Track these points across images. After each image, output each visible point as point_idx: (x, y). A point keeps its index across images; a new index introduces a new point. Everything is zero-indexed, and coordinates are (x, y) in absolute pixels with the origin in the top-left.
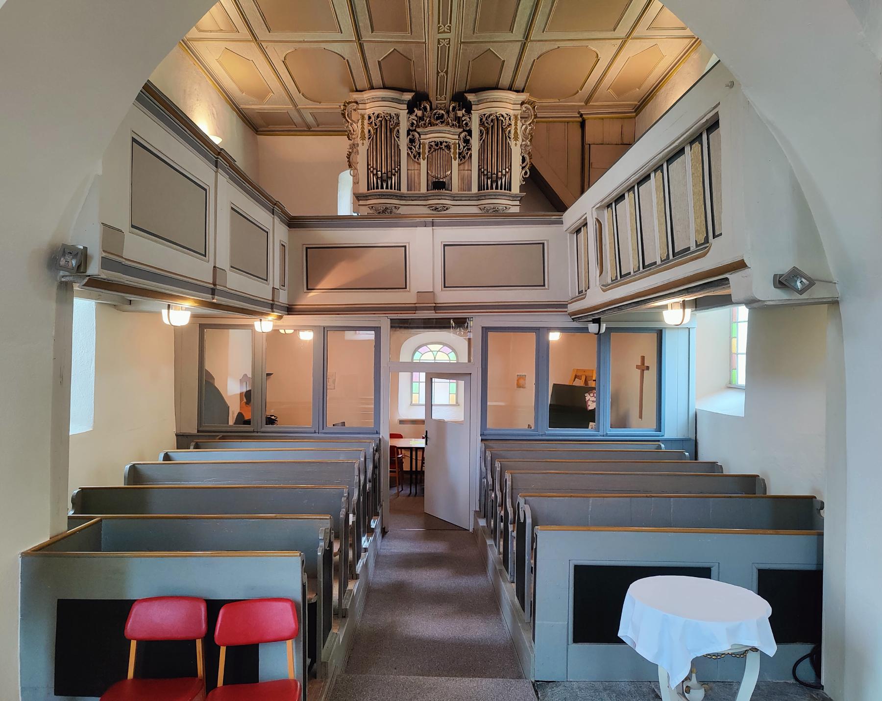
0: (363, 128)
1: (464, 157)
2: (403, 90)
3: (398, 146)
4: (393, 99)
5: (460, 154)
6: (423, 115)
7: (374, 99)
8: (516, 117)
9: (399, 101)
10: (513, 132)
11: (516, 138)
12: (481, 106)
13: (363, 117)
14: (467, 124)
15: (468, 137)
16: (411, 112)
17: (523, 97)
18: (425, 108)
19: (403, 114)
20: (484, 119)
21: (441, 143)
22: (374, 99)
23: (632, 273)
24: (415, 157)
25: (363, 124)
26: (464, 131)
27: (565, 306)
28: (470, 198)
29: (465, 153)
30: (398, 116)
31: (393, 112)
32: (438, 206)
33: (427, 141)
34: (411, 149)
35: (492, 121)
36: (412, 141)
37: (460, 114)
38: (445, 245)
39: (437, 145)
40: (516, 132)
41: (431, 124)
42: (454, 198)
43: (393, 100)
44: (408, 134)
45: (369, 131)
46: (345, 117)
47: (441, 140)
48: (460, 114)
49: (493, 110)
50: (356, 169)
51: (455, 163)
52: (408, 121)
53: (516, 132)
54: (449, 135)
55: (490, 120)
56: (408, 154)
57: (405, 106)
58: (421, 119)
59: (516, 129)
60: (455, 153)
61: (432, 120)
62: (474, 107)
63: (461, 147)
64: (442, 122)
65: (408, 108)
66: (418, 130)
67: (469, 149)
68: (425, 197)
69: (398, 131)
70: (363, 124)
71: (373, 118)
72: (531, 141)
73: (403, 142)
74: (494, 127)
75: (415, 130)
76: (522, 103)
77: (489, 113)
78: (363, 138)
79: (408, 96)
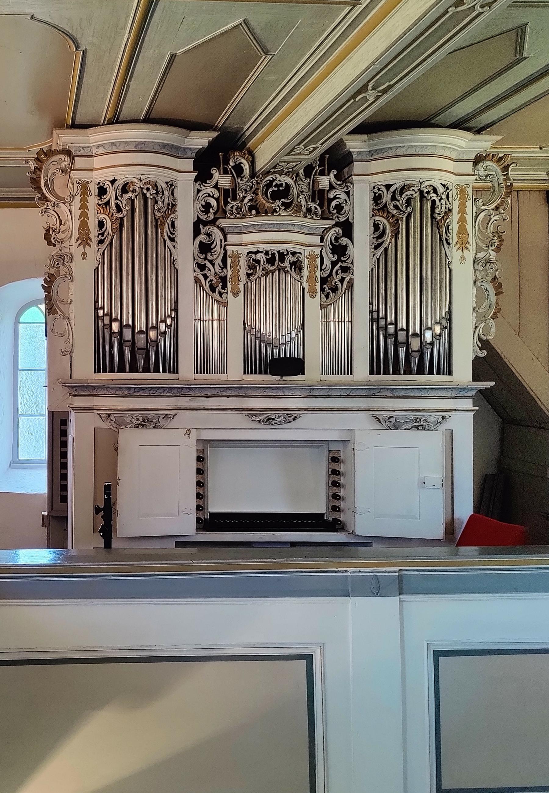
0: (84, 216)
3: (173, 262)
4: (164, 146)
5: (324, 281)
7: (116, 149)
8: (462, 191)
9: (175, 151)
10: (454, 227)
11: (463, 244)
12: (375, 166)
13: (84, 188)
14: (339, 208)
15: (344, 241)
16: (203, 176)
17: (484, 143)
18: (239, 169)
19: (186, 182)
20: (387, 197)
21: (282, 257)
22: (116, 149)
23: (313, 373)
24: (213, 289)
25: (84, 206)
28: (350, 392)
30: (171, 185)
31: (161, 178)
32: (273, 414)
34: (202, 267)
35: (408, 202)
36: (205, 248)
37: (323, 182)
38: (438, 654)
39: (271, 261)
40: (462, 230)
41: (256, 208)
42: (312, 392)
44: (197, 232)
45: (101, 224)
46: (38, 188)
47: (282, 248)
48: (323, 182)
49: (412, 177)
50: (66, 317)
52: (197, 197)
53: (462, 230)
54: (299, 234)
55: (403, 200)
57: (189, 164)
58: (228, 194)
59: (462, 220)
60: (311, 279)
61: (261, 198)
62: (358, 167)
64: (287, 206)
65: (195, 168)
66: (223, 223)
67: (345, 270)
68: (239, 391)
69: (173, 225)
70: (84, 206)
71: (111, 194)
72: (498, 250)
73: (186, 249)
74: (408, 213)
75: (213, 222)
76: (478, 160)
78: (84, 240)
79: (200, 140)
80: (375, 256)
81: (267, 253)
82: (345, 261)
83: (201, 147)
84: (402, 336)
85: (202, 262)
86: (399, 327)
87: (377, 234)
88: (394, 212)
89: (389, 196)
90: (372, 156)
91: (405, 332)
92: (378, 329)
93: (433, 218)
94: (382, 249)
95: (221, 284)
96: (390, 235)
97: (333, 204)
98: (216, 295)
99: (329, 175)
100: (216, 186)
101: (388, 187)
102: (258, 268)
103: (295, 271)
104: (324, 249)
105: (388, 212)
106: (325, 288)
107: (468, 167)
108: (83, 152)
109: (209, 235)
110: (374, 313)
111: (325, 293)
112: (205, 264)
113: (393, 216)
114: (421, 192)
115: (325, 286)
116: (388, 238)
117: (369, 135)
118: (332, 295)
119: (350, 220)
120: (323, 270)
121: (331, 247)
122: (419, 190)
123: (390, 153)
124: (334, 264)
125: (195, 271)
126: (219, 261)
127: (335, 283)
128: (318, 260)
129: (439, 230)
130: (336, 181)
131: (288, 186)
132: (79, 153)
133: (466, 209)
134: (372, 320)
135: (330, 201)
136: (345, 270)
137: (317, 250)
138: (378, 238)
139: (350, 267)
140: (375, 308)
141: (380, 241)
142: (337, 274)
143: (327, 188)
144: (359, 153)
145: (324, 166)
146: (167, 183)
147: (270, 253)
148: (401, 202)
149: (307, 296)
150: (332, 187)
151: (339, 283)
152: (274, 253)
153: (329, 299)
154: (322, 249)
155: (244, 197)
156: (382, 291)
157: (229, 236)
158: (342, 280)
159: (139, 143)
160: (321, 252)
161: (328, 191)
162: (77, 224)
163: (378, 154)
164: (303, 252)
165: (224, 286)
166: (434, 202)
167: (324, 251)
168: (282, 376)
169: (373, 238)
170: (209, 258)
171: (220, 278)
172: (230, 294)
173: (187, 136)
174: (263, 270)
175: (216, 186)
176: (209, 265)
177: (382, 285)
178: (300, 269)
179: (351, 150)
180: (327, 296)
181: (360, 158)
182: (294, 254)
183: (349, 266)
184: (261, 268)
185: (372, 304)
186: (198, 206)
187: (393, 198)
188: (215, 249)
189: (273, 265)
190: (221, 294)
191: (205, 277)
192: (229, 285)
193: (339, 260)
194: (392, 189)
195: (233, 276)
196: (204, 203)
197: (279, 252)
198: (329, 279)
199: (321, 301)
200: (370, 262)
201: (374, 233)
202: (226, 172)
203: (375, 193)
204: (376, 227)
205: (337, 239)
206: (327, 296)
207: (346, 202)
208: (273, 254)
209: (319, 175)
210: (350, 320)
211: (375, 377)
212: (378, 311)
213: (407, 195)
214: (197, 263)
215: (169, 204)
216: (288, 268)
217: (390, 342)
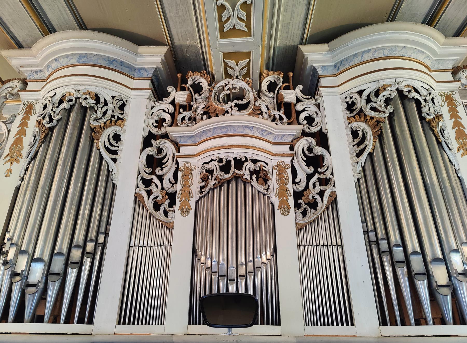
1: (311, 202)
2: (139, 40)
4: (112, 61)
5: (298, 195)
6: (191, 98)
14: (310, 120)
15: (319, 150)
16: (159, 93)
20: (361, 103)
21: (239, 163)
24: (157, 206)
26: (304, 134)
27: (213, 131)
29: (313, 192)
33: (197, 163)
34: (147, 183)
35: (388, 101)
36: (154, 163)
37: (289, 96)
39: (226, 168)
43: (112, 64)
44: (147, 142)
47: (240, 154)
48: (289, 96)
49: (385, 78)
51: (286, 224)
56: (137, 197)
57: (147, 84)
60: (282, 193)
61: (215, 104)
62: (324, 82)
63: (301, 175)
64: (241, 108)
67: (325, 182)
69: (117, 137)
73: (128, 167)
75: (165, 136)
77: (374, 87)
80: (359, 164)
81: (220, 161)
82: (323, 173)
83: (155, 66)
84: (417, 263)
85: (148, 177)
86: (410, 249)
87: (357, 141)
88: (372, 114)
89: (364, 101)
90: (338, 70)
91: (421, 257)
92: (380, 253)
93: (422, 119)
94: (365, 155)
95: (168, 201)
96: (372, 137)
97: (303, 116)
98: (160, 215)
99: (295, 90)
100: (173, 103)
101: (360, 93)
102: (210, 178)
103: (257, 180)
104: (295, 158)
105: (366, 116)
106: (301, 203)
107: (448, 76)
108: (36, 77)
109: (160, 150)
110: (370, 234)
111: (302, 210)
112: (152, 179)
113: (372, 118)
114: (400, 92)
115: (300, 201)
116: (370, 143)
117: (329, 44)
118: (311, 212)
119: (324, 131)
120: (298, 183)
121: (305, 159)
122: (397, 89)
123: (356, 61)
124: (309, 177)
125: (138, 187)
126: (170, 175)
127: (313, 197)
128: (289, 171)
129: (433, 131)
130: (304, 96)
131: (242, 89)
132: (32, 78)
133: (458, 114)
134: (369, 243)
135: (298, 113)
136: (325, 182)
137: (287, 160)
138: (359, 144)
139: (330, 179)
140: (370, 227)
141: (362, 147)
142: (314, 186)
143: (294, 101)
144: (324, 68)
145: (289, 83)
146: (113, 97)
147: (224, 160)
148: (378, 103)
149: (277, 212)
150: (298, 100)
151: (318, 197)
152: (230, 161)
153: (307, 216)
154: (293, 159)
155: (197, 108)
156: (375, 204)
157: (181, 148)
158: (321, 194)
159: (81, 56)
160: (292, 162)
161: (295, 105)
162: (11, 139)
163: (344, 65)
164: (270, 163)
165: (172, 204)
166: (418, 102)
167: (295, 161)
168: (230, 327)
169: (353, 146)
170: (157, 173)
171: (167, 194)
172: (178, 213)
173: (136, 53)
174: (215, 179)
175: (173, 103)
176: (156, 180)
177: (374, 196)
178: (266, 180)
179: (314, 65)
180: (304, 213)
181: (326, 73)
182: (255, 161)
183: (328, 177)
184: (214, 178)
185: (366, 222)
186: (151, 122)
187: (368, 100)
188: (167, 164)
189: (227, 172)
190: (166, 213)
191: (149, 193)
192: (178, 201)
193: (316, 172)
194: (365, 94)
195: (183, 191)
196: (157, 119)
197: (235, 159)
198: (305, 193)
199: (296, 218)
200: (354, 172)
201: (353, 141)
202: (183, 89)
203: (347, 103)
204: (355, 134)
205: (310, 149)
206: (304, 213)
207: (317, 114)
208: (228, 162)
209: (284, 89)
210: (339, 243)
211: (389, 330)
212: (375, 231)
213: (383, 96)
214: (143, 179)
215: (113, 116)
216: (247, 176)
217: (402, 272)
